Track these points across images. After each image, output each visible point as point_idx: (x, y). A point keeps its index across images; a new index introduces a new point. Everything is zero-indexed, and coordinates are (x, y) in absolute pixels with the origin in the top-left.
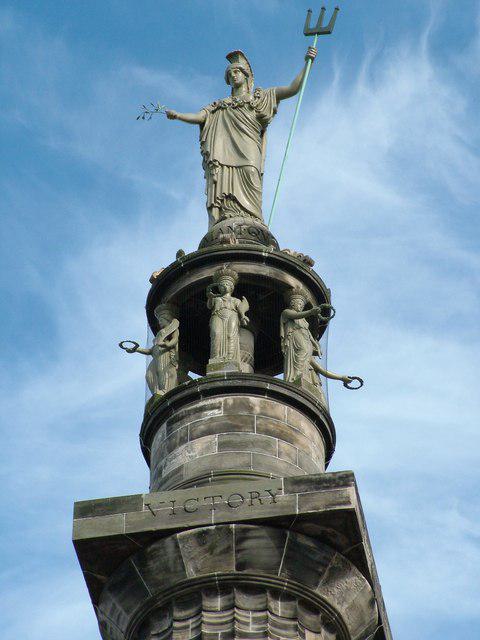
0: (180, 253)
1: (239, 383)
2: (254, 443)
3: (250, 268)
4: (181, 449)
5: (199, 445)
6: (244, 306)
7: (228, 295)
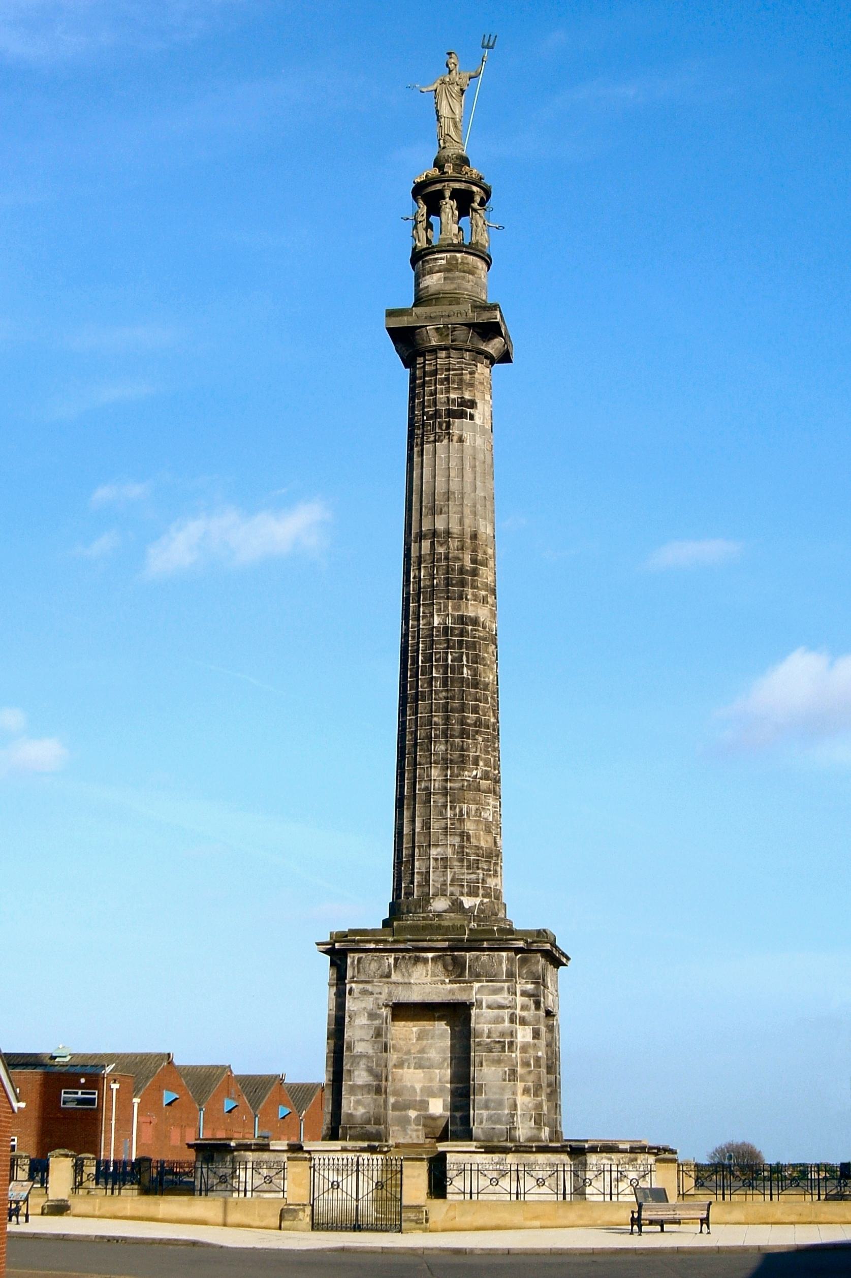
0: (331, 933)
1: (452, 248)
2: (458, 278)
4: (427, 277)
7: (447, 199)
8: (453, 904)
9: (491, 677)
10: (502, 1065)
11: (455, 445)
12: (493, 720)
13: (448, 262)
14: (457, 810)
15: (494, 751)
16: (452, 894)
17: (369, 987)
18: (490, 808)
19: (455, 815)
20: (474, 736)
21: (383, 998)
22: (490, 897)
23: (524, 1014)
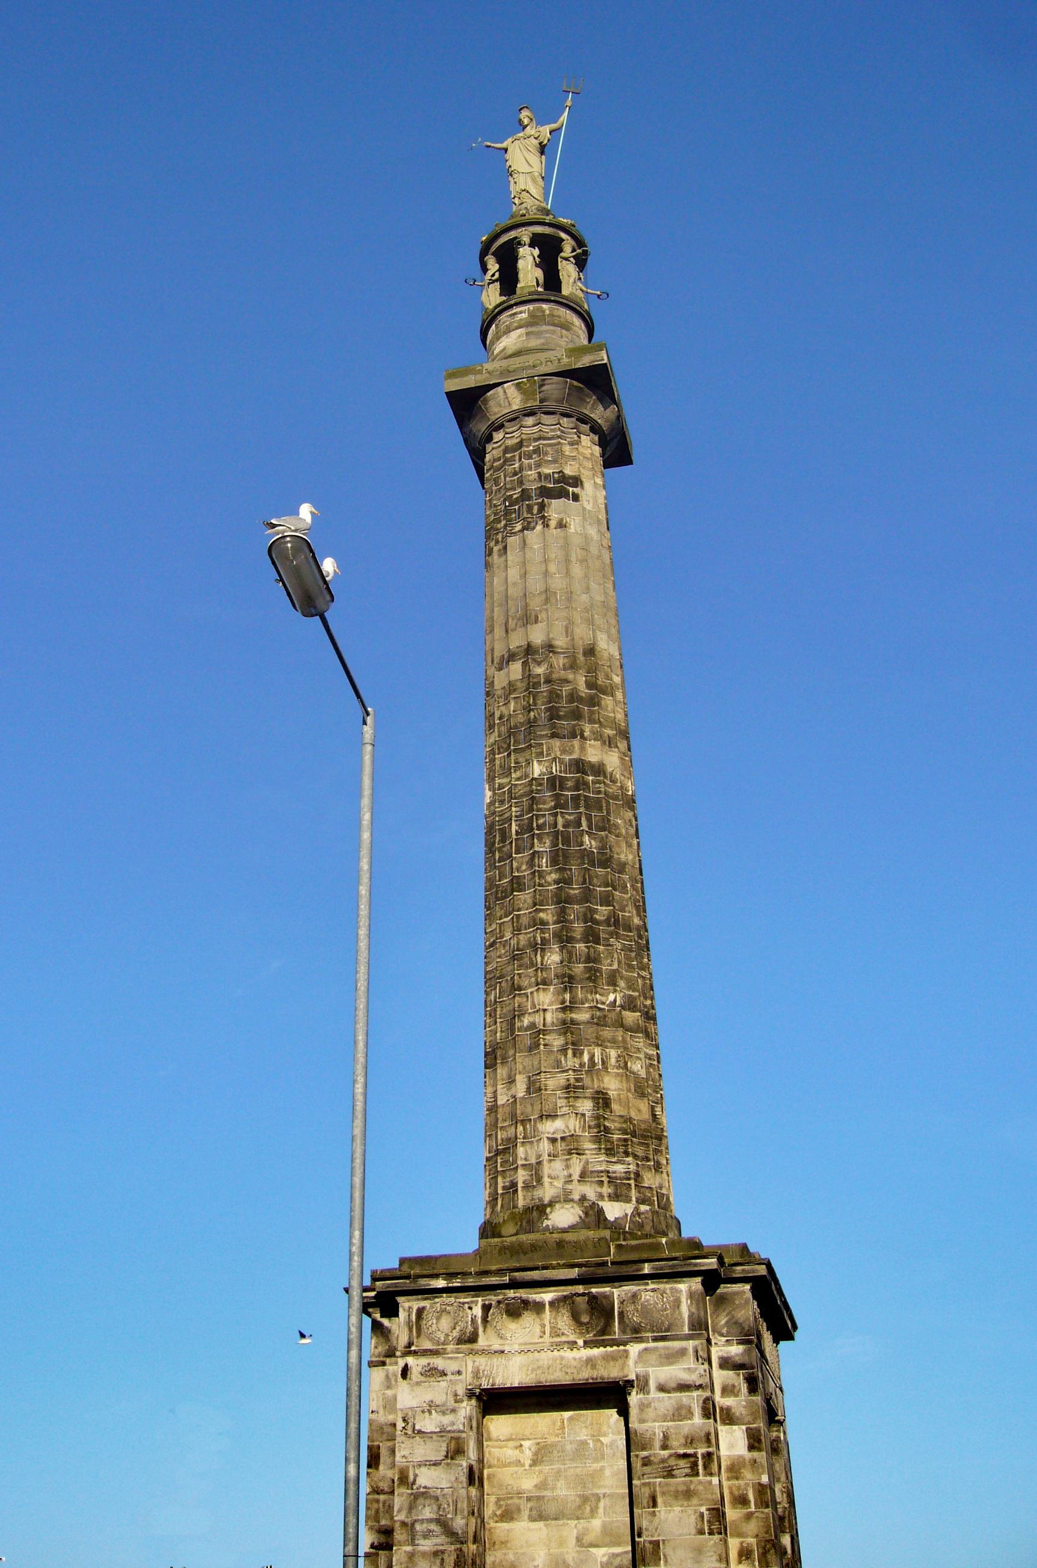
1: (535, 297)
2: (546, 332)
3: (539, 229)
5: (514, 335)
6: (536, 252)
8: (586, 1214)
9: (630, 857)
10: (695, 1501)
11: (553, 531)
12: (636, 921)
13: (532, 315)
14: (586, 1057)
15: (643, 969)
16: (583, 1198)
17: (439, 1362)
18: (642, 1056)
19: (582, 1065)
20: (607, 940)
21: (466, 1380)
22: (651, 1204)
23: (729, 1402)
